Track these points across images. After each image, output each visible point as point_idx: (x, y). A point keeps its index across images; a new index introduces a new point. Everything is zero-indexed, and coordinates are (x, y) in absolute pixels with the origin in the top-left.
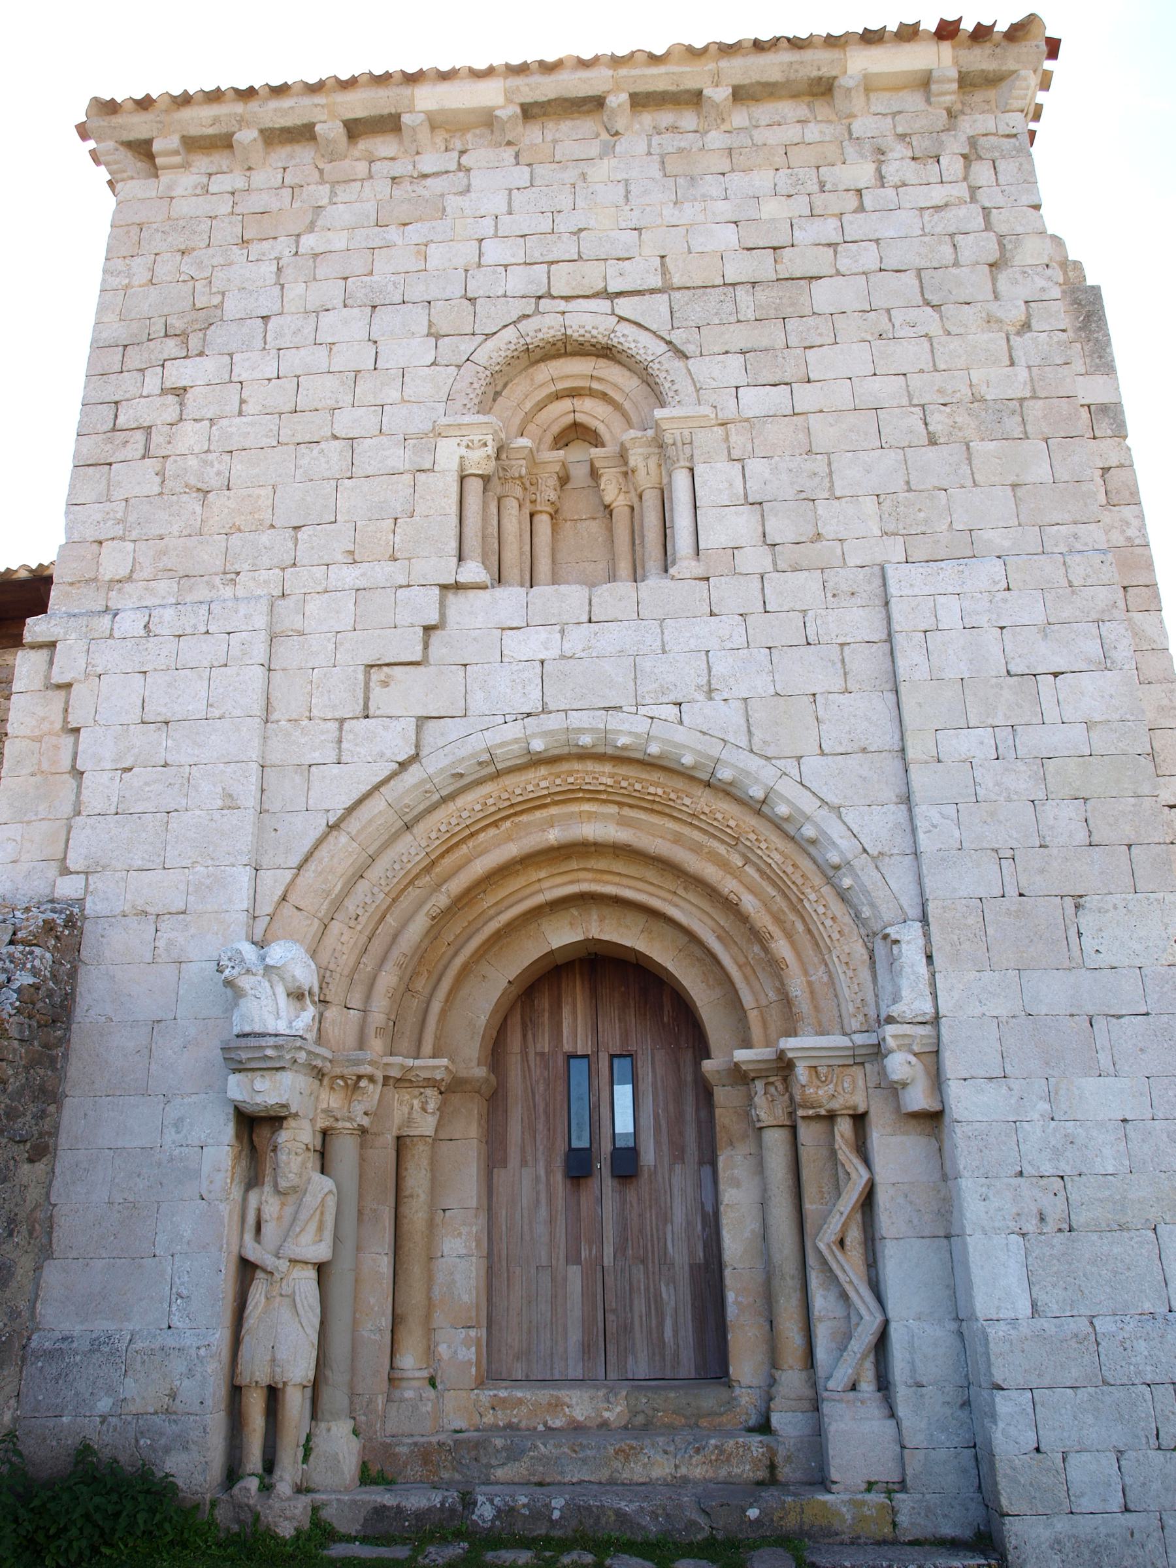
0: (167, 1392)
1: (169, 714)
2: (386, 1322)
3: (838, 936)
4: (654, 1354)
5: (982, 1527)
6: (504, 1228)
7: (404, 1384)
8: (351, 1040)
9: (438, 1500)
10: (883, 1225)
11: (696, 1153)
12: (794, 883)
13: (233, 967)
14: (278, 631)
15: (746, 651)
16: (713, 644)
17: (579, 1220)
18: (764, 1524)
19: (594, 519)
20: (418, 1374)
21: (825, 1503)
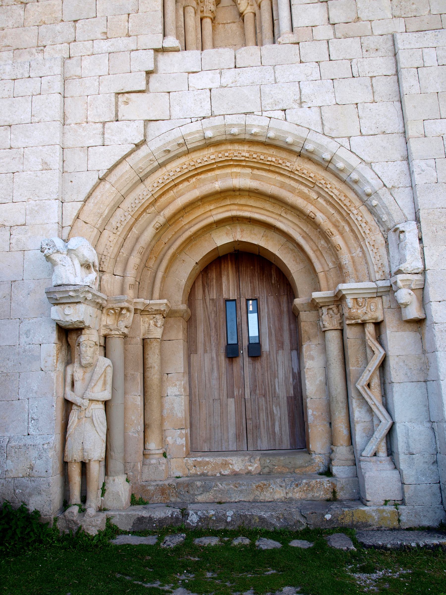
0: (28, 467)
1: (11, 121)
2: (141, 428)
3: (369, 232)
4: (270, 438)
5: (443, 521)
6: (197, 381)
7: (151, 457)
8: (117, 290)
9: (169, 513)
10: (392, 376)
11: (289, 345)
12: (345, 205)
13: (49, 249)
14: (68, 76)
15: (320, 81)
16: (302, 78)
17: (233, 377)
18: (334, 522)
19: (234, 22)
20: (157, 452)
21: (364, 511)
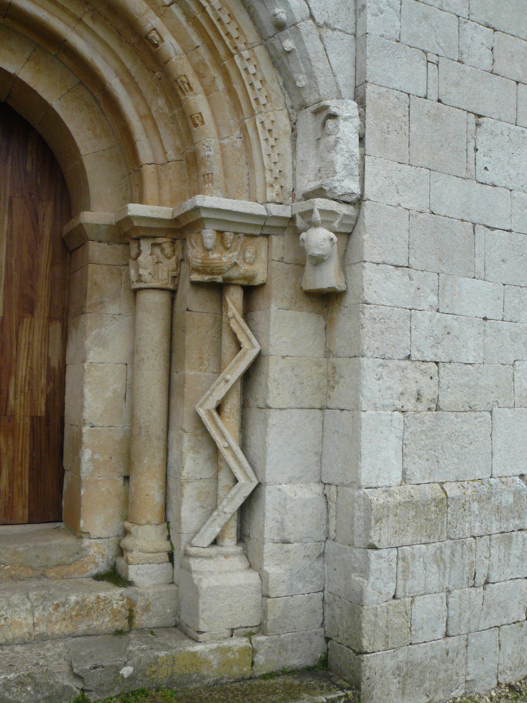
12: (228, 34)
